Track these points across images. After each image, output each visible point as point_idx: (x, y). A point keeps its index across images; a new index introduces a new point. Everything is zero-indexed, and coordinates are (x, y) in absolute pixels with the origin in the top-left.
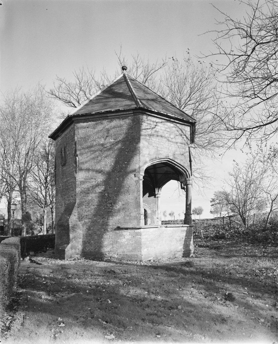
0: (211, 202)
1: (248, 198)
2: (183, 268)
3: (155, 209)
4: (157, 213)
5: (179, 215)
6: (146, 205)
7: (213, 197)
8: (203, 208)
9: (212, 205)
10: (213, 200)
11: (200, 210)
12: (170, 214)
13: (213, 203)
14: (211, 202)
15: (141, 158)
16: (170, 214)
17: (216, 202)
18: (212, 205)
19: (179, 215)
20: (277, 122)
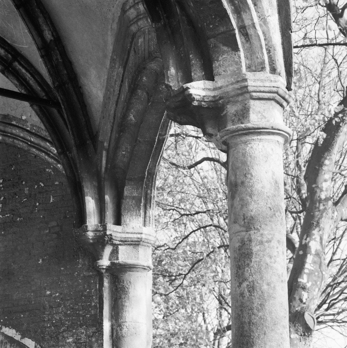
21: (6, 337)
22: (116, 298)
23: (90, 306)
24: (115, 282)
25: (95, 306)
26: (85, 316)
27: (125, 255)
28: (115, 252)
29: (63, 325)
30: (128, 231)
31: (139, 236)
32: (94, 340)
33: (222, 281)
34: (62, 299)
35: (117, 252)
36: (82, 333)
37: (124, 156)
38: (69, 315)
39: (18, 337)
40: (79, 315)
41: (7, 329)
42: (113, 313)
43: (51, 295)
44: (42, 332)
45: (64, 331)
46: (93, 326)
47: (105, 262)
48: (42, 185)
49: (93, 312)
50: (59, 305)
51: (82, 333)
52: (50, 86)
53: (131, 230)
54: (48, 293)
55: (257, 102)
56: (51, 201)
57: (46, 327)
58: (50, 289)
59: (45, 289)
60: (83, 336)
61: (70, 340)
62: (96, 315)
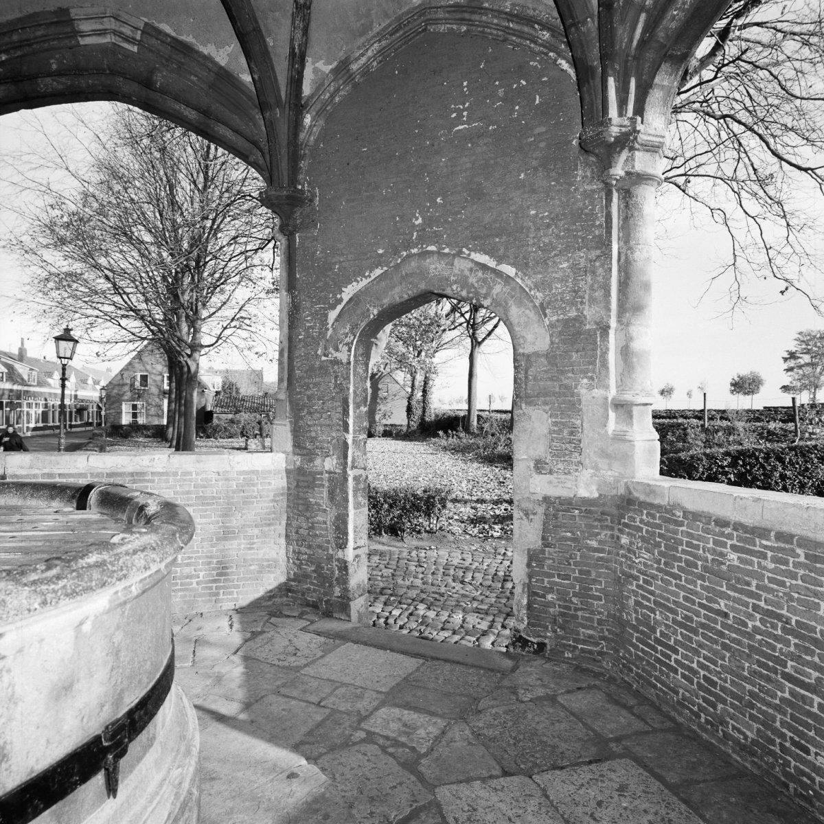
0: (785, 360)
1: (146, 342)
2: (673, 25)
3: (590, 312)
4: (612, 357)
5: (689, 395)
6: (509, 270)
7: (793, 346)
8: (763, 376)
9: (790, 369)
10: (792, 355)
11: (754, 381)
12: (662, 393)
13: (792, 363)
14: (785, 360)
15: (273, 325)
16: (662, 393)
17: (800, 360)
18: (790, 369)
19: (689, 395)
20: (501, 323)
21: (477, 264)
22: (627, 217)
23: (593, 225)
24: (624, 198)
25: (601, 226)
26: (585, 237)
27: (642, 162)
28: (630, 159)
29: (554, 248)
30: (651, 132)
31: (661, 140)
32: (597, 264)
33: (792, 129)
34: (552, 219)
35: (633, 160)
36: (581, 257)
37: (673, 18)
38: (563, 237)
39: (492, 263)
40: (576, 237)
41: (478, 255)
42: (621, 235)
43: (537, 215)
44: (524, 258)
45: (556, 255)
46: (597, 248)
47: (618, 171)
48: (524, 83)
49: (597, 232)
50: (548, 226)
51: (581, 257)
52: (279, 91)
53: (653, 132)
54: (533, 212)
55: (504, 408)
56: (537, 102)
57: (530, 253)
58: (536, 208)
59: (528, 208)
60: (582, 260)
61: (565, 265)
62: (600, 236)
